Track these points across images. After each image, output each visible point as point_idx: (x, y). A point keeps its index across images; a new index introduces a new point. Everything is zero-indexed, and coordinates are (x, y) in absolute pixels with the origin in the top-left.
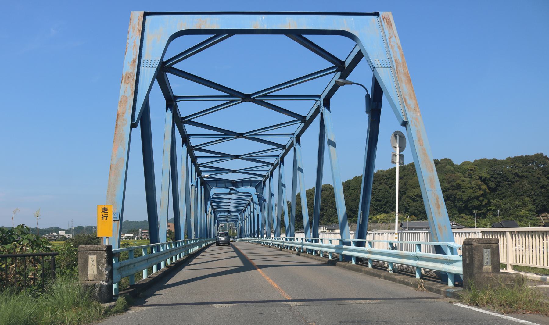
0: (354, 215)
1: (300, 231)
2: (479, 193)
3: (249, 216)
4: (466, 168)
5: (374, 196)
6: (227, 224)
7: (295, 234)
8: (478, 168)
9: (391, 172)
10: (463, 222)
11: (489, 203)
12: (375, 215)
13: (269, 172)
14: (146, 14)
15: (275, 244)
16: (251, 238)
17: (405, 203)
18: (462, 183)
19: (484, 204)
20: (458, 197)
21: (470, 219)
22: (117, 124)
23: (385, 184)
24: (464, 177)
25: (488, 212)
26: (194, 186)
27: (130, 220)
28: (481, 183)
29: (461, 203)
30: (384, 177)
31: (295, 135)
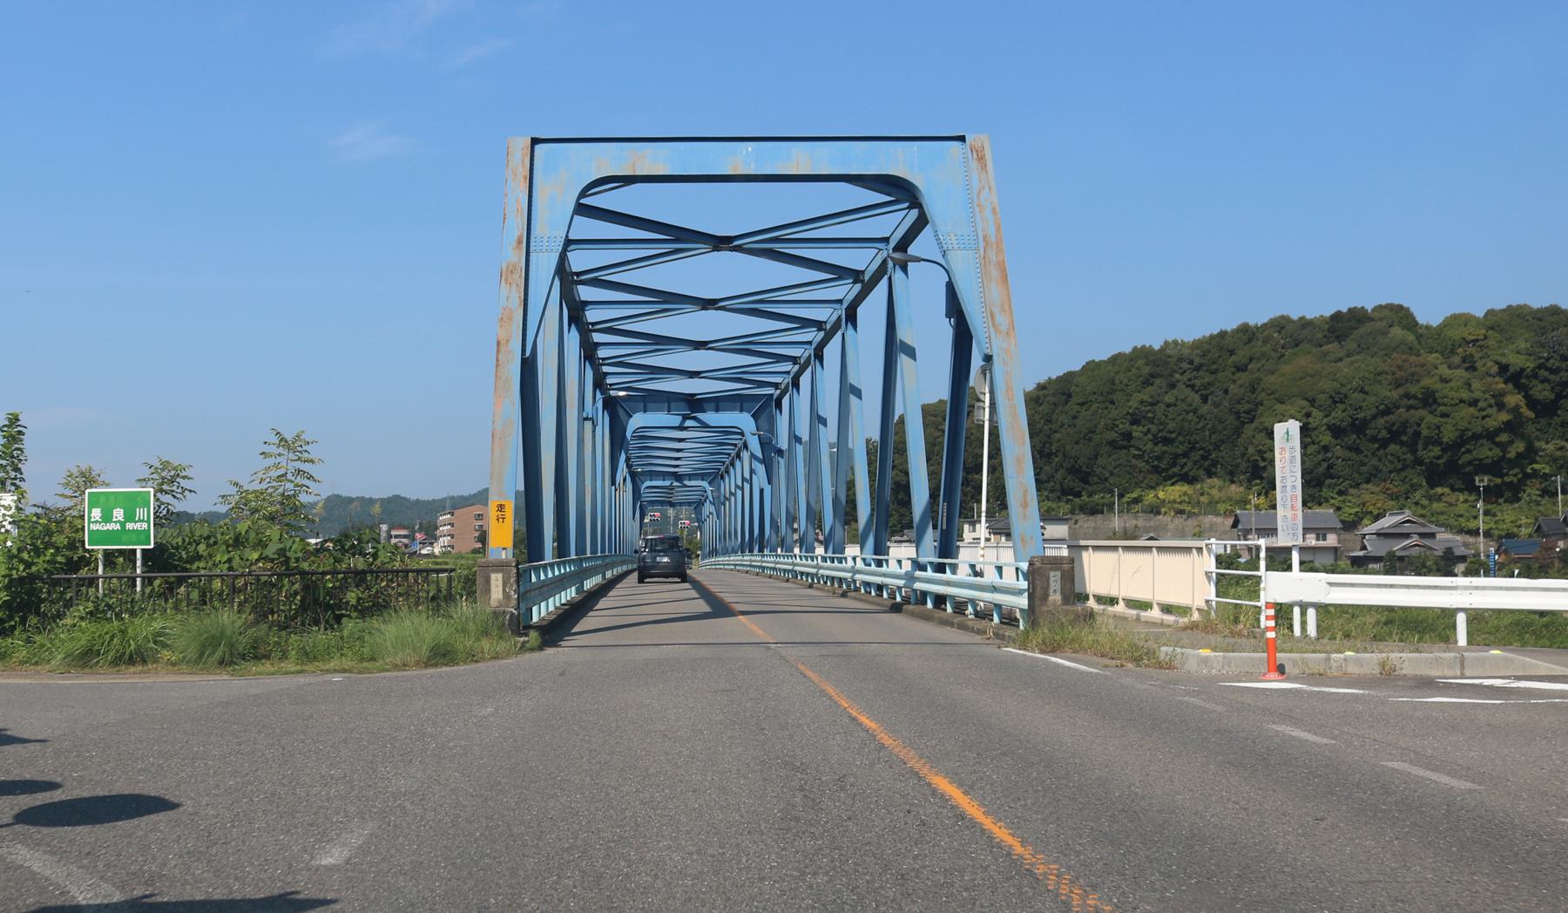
0: (1083, 489)
1: (905, 538)
2: (1495, 420)
3: (738, 490)
4: (1457, 338)
5: (1150, 426)
6: (671, 512)
7: (889, 547)
8: (1496, 335)
9: (1206, 347)
10: (1443, 513)
11: (1530, 454)
12: (1152, 488)
13: (791, 377)
14: (535, 141)
15: (802, 573)
16: (743, 556)
17: (1251, 450)
18: (1439, 386)
19: (1512, 455)
20: (1427, 431)
21: (1466, 505)
22: (497, 360)
23: (1187, 386)
24: (1450, 367)
25: (1528, 483)
26: (592, 419)
27: (344, 494)
28: (1503, 386)
29: (1436, 451)
30: (1185, 365)
31: (845, 305)
